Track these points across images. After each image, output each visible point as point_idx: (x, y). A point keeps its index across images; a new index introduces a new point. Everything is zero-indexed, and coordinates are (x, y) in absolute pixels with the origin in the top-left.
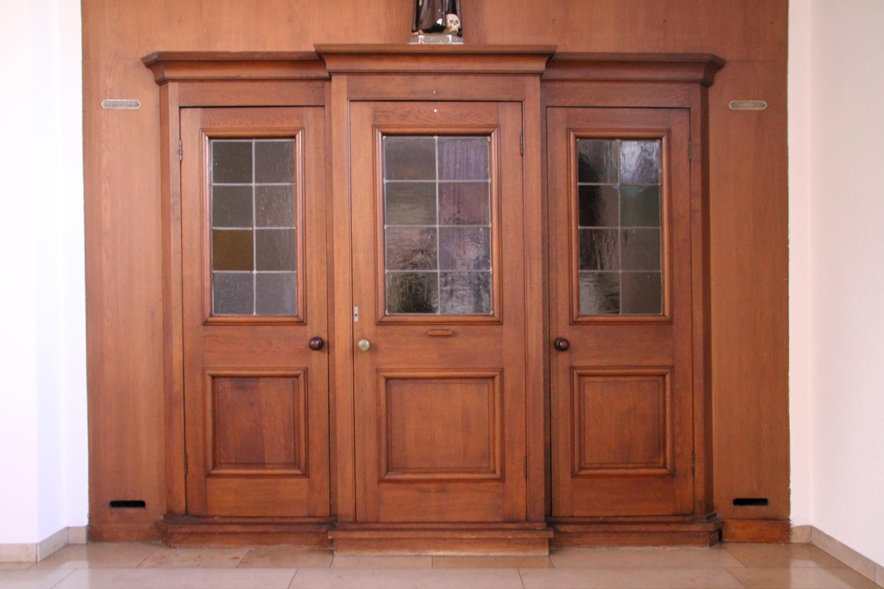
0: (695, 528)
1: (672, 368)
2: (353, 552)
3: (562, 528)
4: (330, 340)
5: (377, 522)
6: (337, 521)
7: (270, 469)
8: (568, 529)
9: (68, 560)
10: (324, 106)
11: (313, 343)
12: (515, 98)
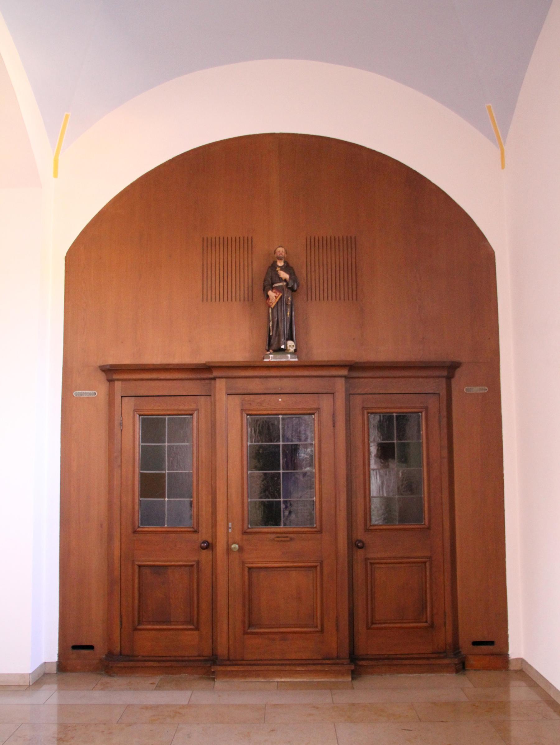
0: (446, 661)
1: (430, 558)
2: (228, 680)
3: (361, 663)
4: (214, 542)
5: (243, 660)
6: (217, 659)
7: (174, 625)
8: (364, 663)
9: (45, 683)
10: (211, 396)
11: (202, 545)
12: (329, 391)
